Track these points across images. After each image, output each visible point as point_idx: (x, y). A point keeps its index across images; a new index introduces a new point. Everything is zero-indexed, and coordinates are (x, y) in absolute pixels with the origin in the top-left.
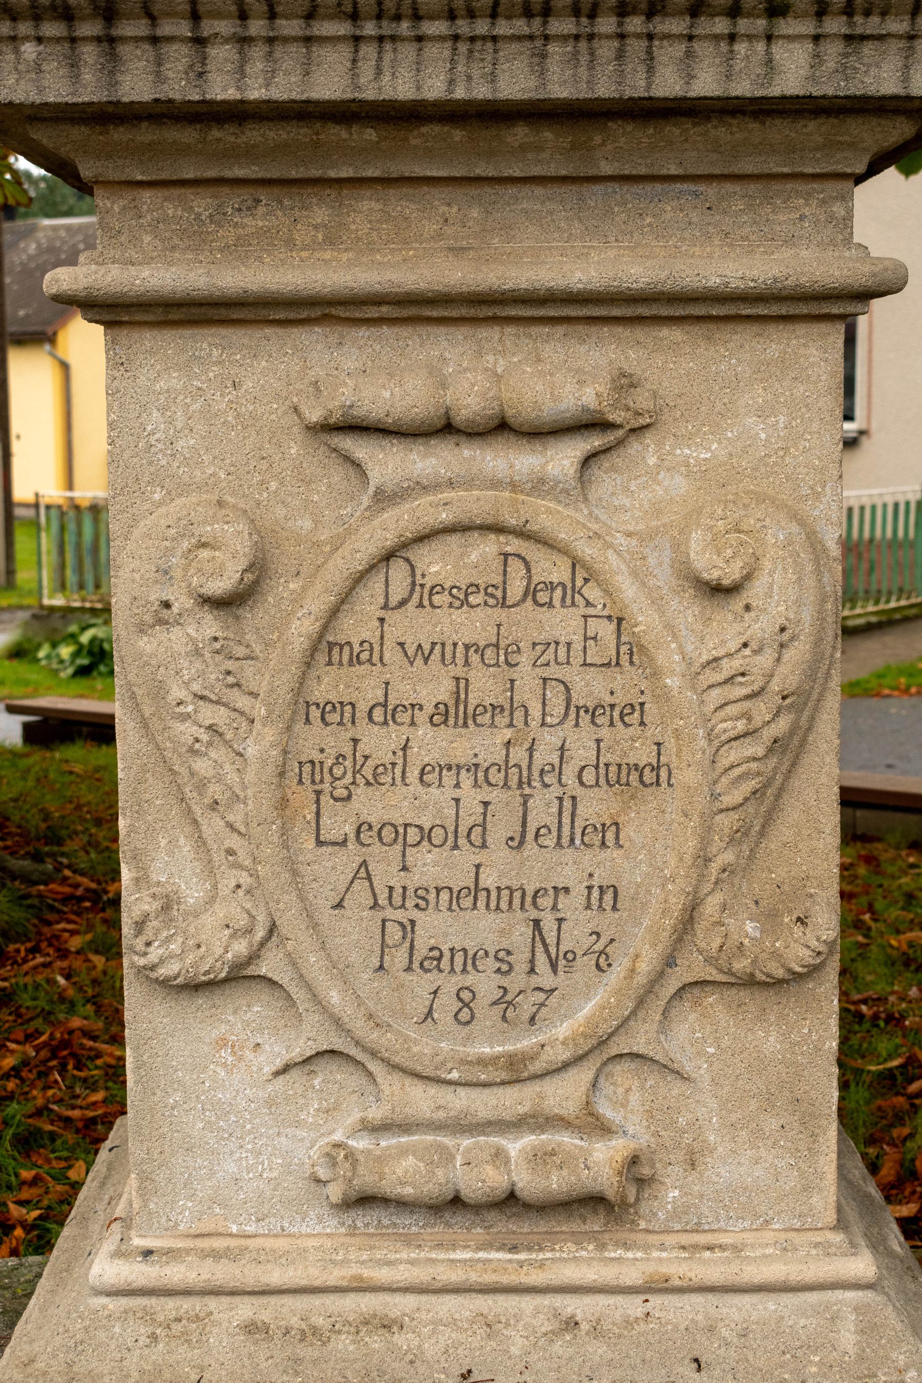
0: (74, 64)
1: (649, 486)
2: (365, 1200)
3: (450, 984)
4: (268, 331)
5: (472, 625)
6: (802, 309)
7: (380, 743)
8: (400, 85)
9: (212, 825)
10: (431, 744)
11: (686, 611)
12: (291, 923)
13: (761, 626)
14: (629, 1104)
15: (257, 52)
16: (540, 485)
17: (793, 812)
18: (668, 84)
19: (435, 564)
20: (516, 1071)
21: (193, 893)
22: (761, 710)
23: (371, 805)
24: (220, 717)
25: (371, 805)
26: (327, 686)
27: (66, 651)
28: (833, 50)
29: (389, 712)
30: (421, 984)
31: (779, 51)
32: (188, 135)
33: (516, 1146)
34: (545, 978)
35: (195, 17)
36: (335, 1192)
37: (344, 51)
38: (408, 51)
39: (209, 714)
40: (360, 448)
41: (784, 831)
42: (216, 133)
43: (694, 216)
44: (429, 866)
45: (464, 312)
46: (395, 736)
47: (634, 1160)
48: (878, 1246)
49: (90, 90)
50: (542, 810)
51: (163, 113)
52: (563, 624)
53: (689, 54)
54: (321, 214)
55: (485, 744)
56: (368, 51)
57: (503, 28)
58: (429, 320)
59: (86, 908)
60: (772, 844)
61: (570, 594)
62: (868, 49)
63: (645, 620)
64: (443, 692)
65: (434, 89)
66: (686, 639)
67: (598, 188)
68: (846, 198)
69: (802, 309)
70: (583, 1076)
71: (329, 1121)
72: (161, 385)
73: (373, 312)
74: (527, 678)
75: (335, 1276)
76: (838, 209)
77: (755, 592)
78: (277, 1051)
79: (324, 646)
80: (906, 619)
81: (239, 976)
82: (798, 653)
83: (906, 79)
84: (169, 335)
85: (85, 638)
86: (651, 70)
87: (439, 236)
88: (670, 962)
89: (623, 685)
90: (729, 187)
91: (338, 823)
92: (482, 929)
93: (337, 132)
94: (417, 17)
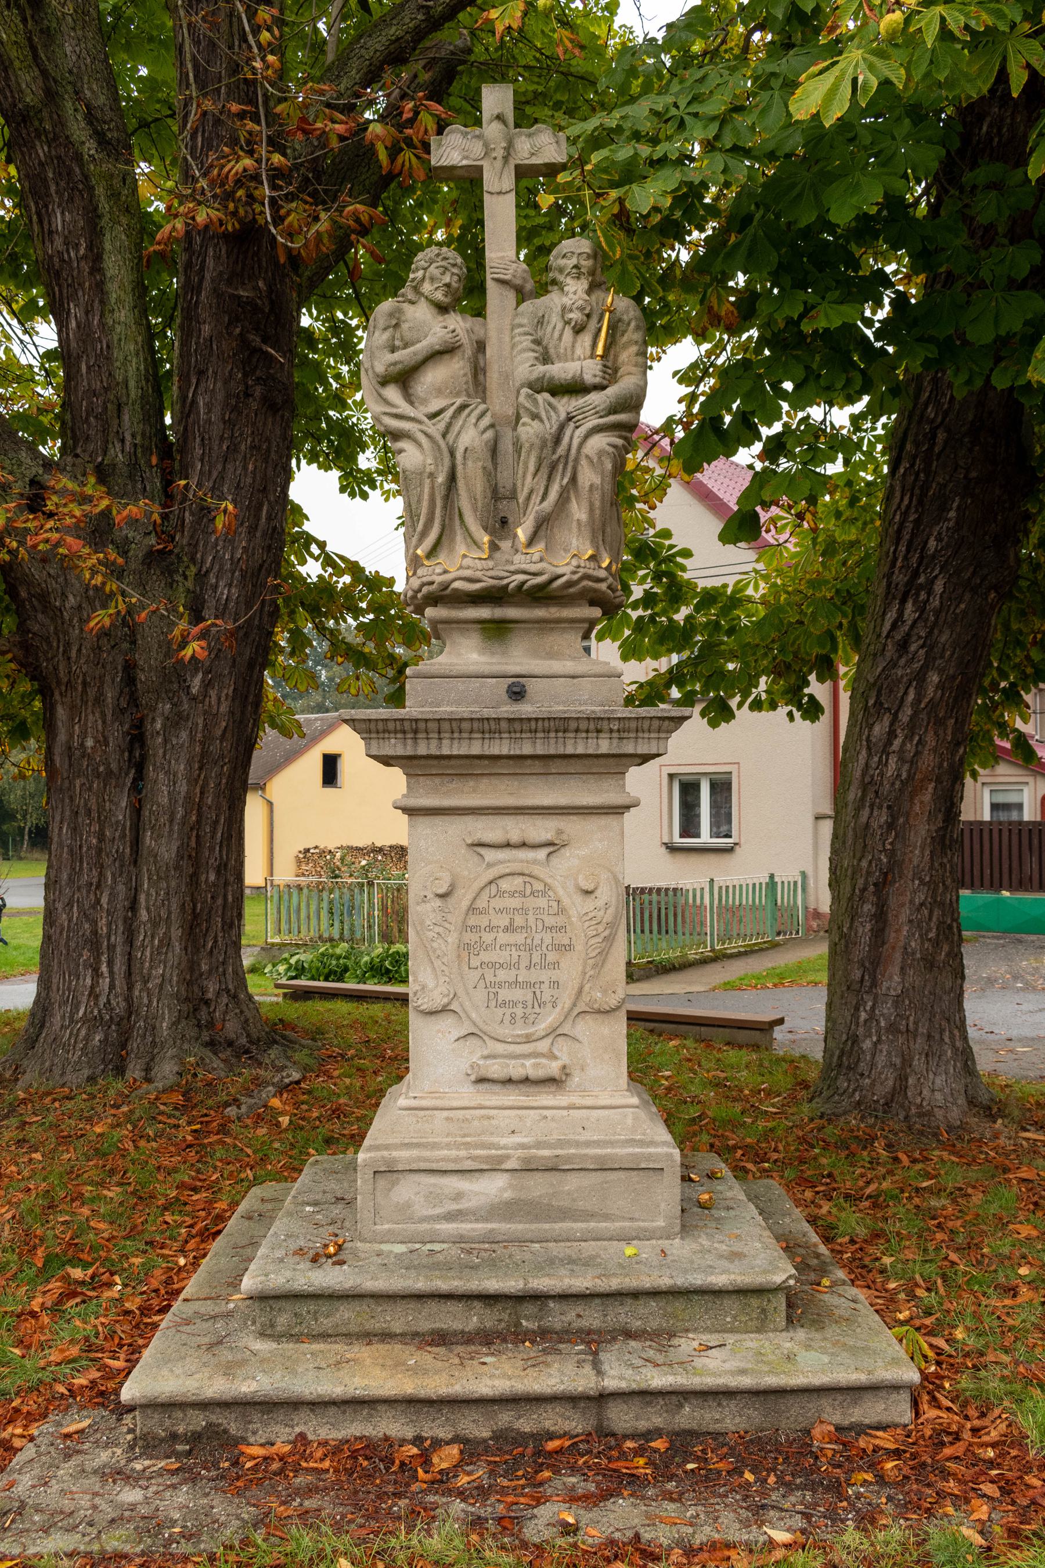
1: (567, 862)
2: (481, 1080)
3: (508, 1012)
5: (515, 903)
7: (488, 938)
8: (495, 750)
9: (437, 963)
10: (503, 938)
11: (578, 898)
12: (461, 992)
13: (600, 903)
14: (564, 1052)
16: (535, 862)
17: (611, 960)
18: (570, 750)
19: (504, 885)
20: (528, 1039)
21: (431, 984)
22: (601, 928)
23: (485, 957)
24: (440, 930)
25: (485, 957)
26: (472, 921)
27: (282, 968)
28: (615, 741)
29: (491, 928)
30: (500, 1011)
33: (529, 1063)
34: (537, 1010)
36: (473, 1078)
39: (437, 929)
40: (482, 851)
41: (608, 966)
44: (502, 975)
46: (492, 935)
47: (564, 1067)
48: (639, 1095)
49: (409, 751)
50: (536, 958)
51: (429, 757)
52: (542, 902)
54: (471, 783)
55: (519, 938)
59: (733, 656)
60: (605, 969)
61: (544, 894)
63: (566, 901)
64: (507, 923)
65: (505, 751)
66: (577, 907)
70: (548, 1041)
71: (472, 1055)
74: (531, 919)
75: (472, 1104)
77: (598, 893)
78: (456, 1034)
79: (472, 909)
80: (761, 950)
81: (444, 1010)
82: (611, 911)
85: (293, 961)
88: (574, 1005)
89: (560, 920)
91: (475, 962)
92: (518, 994)
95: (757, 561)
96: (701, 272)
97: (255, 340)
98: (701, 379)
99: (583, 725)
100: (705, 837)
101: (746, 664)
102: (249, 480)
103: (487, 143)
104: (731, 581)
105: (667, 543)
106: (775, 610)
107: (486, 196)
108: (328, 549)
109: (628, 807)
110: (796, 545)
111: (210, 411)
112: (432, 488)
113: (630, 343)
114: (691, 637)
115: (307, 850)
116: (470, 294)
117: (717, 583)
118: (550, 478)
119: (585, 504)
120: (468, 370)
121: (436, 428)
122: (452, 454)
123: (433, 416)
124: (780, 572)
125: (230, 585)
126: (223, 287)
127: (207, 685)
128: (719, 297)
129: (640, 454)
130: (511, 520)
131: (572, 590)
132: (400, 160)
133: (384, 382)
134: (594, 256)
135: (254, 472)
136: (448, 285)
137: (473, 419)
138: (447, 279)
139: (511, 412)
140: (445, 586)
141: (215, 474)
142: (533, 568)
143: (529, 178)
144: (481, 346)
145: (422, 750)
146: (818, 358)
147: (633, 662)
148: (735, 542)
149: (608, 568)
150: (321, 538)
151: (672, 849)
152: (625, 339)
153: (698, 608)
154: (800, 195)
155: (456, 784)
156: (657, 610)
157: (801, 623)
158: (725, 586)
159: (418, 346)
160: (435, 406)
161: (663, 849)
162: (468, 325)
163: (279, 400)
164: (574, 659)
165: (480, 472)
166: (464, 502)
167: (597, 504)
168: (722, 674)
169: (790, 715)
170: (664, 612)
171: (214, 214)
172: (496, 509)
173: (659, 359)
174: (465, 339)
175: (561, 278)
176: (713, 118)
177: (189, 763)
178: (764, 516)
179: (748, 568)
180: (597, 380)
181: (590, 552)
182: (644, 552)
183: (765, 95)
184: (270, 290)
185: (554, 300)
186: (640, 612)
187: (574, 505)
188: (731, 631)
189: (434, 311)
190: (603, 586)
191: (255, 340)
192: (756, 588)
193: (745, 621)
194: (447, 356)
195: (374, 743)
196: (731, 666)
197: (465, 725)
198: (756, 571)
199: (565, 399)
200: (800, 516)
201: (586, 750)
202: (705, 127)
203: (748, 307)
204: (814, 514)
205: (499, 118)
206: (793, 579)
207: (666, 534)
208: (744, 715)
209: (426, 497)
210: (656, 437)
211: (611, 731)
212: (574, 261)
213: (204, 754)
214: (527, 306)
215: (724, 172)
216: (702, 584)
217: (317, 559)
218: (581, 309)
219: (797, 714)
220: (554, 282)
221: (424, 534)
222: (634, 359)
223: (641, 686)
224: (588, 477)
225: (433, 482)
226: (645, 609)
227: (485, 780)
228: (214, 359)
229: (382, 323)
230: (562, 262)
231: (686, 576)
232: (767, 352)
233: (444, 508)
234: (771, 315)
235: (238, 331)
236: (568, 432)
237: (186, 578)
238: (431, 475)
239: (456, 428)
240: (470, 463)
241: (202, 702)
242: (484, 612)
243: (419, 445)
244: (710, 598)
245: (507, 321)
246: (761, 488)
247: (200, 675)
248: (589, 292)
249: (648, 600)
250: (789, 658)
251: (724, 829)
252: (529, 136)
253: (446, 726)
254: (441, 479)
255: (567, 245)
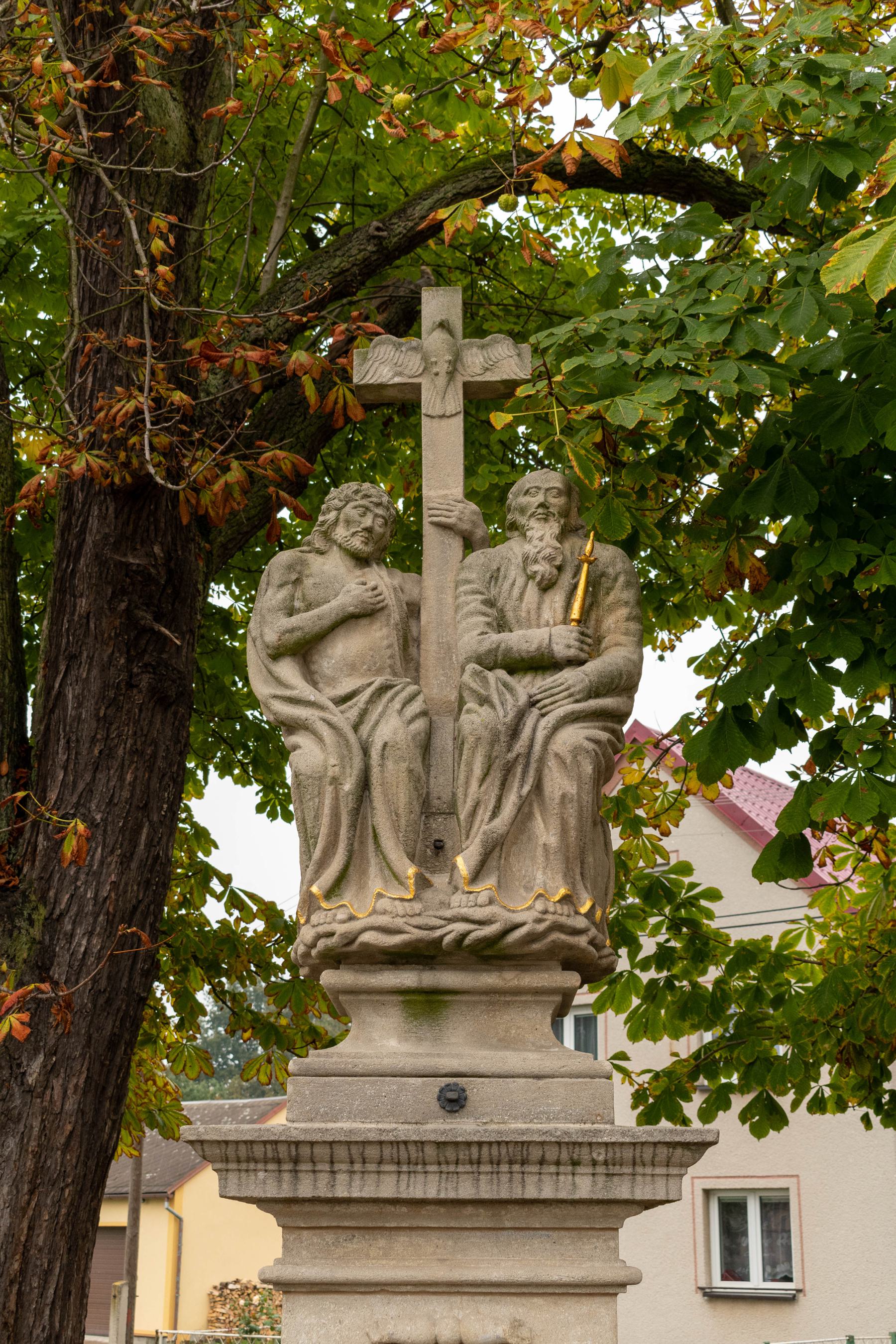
0: (280, 1181)
4: (357, 1296)
6: (597, 1290)
8: (418, 1193)
15: (357, 1177)
18: (531, 1193)
28: (601, 1179)
31: (578, 1179)
32: (325, 1208)
35: (332, 1162)
37: (394, 1177)
38: (421, 1178)
42: (337, 1208)
43: (548, 1246)
45: (444, 1289)
49: (286, 1192)
53: (540, 1180)
54: (382, 1242)
56: (404, 1177)
57: (461, 1169)
58: (429, 1293)
59: (783, 1038)
62: (615, 1179)
65: (432, 1193)
67: (505, 1233)
68: (615, 1238)
69: (597, 1290)
72: (307, 1321)
73: (404, 1289)
76: (612, 1244)
83: (632, 1192)
84: (312, 1297)
86: (524, 1187)
87: (434, 1253)
90: (563, 1233)
93: (391, 1208)
94: (425, 1164)
95: (810, 906)
96: (715, 516)
97: (146, 617)
98: (726, 668)
99: (552, 1154)
100: (756, 1280)
101: (800, 1049)
102: (126, 794)
103: (427, 360)
104: (776, 933)
105: (687, 880)
106: (836, 973)
107: (425, 421)
108: (234, 884)
109: (623, 1285)
110: (861, 885)
111: (80, 705)
112: (336, 799)
113: (618, 604)
114: (723, 1010)
115: (225, 1286)
116: (399, 545)
117: (756, 934)
118: (504, 785)
119: (554, 823)
120: (394, 639)
121: (343, 718)
122: (366, 751)
123: (342, 700)
124: (841, 921)
125: (91, 934)
126: (107, 552)
127: (49, 1072)
128: (741, 551)
129: (647, 763)
130: (449, 844)
131: (536, 946)
132: (332, 397)
133: (277, 655)
134: (568, 491)
135: (133, 784)
136: (369, 530)
137: (397, 705)
138: (368, 521)
139: (453, 696)
140: (350, 939)
141: (81, 786)
142: (479, 913)
143: (480, 399)
144: (413, 610)
145: (305, 1190)
146: (879, 629)
147: (645, 1043)
148: (777, 878)
149: (589, 915)
150: (225, 871)
151: (712, 1296)
152: (611, 598)
153: (731, 970)
154: (844, 418)
155: (358, 1243)
156: (676, 971)
157: (874, 990)
158: (767, 939)
159: (325, 607)
160: (346, 686)
161: (699, 1297)
162: (396, 582)
163: (172, 693)
164: (539, 1048)
165: (404, 775)
166: (381, 819)
167: (572, 822)
168: (770, 1062)
169: (866, 1119)
170: (686, 974)
171: (96, 463)
172: (427, 828)
173: (672, 648)
174: (390, 599)
175: (522, 520)
176: (725, 320)
177: (16, 1184)
178: (815, 846)
179: (799, 914)
180: (572, 652)
181: (562, 891)
182: (657, 892)
183: (793, 291)
184: (169, 558)
185: (514, 549)
186: (652, 974)
187: (538, 823)
188: (778, 1001)
189: (350, 563)
190: (582, 941)
191: (146, 617)
192: (811, 941)
193: (797, 988)
194: (364, 622)
195: (232, 1177)
196: (781, 1050)
197: (372, 1152)
198: (810, 919)
199: (528, 678)
200: (866, 845)
201: (561, 1192)
202: (712, 330)
203: (781, 561)
204: (885, 843)
205: (443, 325)
206: (860, 930)
207: (685, 868)
208: (800, 1118)
209: (327, 810)
210: (667, 743)
211: (594, 1163)
212: (540, 498)
213: (39, 1170)
214: (477, 557)
215: (738, 380)
216: (736, 936)
217: (219, 898)
218: (550, 559)
219: (875, 1120)
220: (514, 526)
221: (322, 864)
222: (624, 625)
223: (657, 1076)
224: (558, 783)
225: (337, 791)
226: (659, 969)
227: (403, 1239)
228: (90, 640)
229: (276, 578)
230: (523, 500)
231: (714, 924)
232: (809, 622)
233: (353, 826)
234: (811, 572)
235: (123, 606)
236: (530, 722)
237: (31, 923)
238: (335, 781)
239: (373, 716)
240: (390, 765)
241: (42, 1096)
242: (408, 978)
243: (320, 739)
244: (747, 955)
245: (450, 578)
246: (810, 803)
247: (41, 1058)
248: (562, 536)
249: (663, 958)
250: (861, 1040)
251: (781, 1269)
252: (483, 347)
253: (341, 1152)
254: (348, 786)
255: (530, 479)
